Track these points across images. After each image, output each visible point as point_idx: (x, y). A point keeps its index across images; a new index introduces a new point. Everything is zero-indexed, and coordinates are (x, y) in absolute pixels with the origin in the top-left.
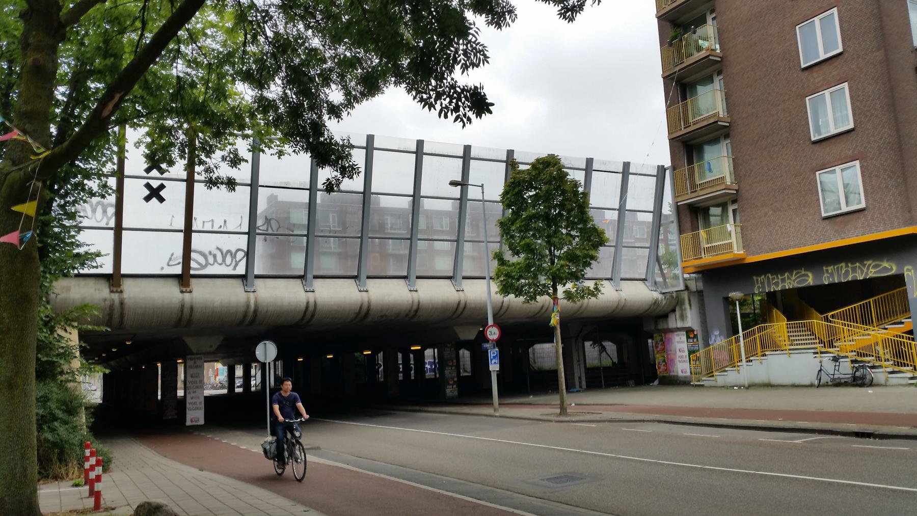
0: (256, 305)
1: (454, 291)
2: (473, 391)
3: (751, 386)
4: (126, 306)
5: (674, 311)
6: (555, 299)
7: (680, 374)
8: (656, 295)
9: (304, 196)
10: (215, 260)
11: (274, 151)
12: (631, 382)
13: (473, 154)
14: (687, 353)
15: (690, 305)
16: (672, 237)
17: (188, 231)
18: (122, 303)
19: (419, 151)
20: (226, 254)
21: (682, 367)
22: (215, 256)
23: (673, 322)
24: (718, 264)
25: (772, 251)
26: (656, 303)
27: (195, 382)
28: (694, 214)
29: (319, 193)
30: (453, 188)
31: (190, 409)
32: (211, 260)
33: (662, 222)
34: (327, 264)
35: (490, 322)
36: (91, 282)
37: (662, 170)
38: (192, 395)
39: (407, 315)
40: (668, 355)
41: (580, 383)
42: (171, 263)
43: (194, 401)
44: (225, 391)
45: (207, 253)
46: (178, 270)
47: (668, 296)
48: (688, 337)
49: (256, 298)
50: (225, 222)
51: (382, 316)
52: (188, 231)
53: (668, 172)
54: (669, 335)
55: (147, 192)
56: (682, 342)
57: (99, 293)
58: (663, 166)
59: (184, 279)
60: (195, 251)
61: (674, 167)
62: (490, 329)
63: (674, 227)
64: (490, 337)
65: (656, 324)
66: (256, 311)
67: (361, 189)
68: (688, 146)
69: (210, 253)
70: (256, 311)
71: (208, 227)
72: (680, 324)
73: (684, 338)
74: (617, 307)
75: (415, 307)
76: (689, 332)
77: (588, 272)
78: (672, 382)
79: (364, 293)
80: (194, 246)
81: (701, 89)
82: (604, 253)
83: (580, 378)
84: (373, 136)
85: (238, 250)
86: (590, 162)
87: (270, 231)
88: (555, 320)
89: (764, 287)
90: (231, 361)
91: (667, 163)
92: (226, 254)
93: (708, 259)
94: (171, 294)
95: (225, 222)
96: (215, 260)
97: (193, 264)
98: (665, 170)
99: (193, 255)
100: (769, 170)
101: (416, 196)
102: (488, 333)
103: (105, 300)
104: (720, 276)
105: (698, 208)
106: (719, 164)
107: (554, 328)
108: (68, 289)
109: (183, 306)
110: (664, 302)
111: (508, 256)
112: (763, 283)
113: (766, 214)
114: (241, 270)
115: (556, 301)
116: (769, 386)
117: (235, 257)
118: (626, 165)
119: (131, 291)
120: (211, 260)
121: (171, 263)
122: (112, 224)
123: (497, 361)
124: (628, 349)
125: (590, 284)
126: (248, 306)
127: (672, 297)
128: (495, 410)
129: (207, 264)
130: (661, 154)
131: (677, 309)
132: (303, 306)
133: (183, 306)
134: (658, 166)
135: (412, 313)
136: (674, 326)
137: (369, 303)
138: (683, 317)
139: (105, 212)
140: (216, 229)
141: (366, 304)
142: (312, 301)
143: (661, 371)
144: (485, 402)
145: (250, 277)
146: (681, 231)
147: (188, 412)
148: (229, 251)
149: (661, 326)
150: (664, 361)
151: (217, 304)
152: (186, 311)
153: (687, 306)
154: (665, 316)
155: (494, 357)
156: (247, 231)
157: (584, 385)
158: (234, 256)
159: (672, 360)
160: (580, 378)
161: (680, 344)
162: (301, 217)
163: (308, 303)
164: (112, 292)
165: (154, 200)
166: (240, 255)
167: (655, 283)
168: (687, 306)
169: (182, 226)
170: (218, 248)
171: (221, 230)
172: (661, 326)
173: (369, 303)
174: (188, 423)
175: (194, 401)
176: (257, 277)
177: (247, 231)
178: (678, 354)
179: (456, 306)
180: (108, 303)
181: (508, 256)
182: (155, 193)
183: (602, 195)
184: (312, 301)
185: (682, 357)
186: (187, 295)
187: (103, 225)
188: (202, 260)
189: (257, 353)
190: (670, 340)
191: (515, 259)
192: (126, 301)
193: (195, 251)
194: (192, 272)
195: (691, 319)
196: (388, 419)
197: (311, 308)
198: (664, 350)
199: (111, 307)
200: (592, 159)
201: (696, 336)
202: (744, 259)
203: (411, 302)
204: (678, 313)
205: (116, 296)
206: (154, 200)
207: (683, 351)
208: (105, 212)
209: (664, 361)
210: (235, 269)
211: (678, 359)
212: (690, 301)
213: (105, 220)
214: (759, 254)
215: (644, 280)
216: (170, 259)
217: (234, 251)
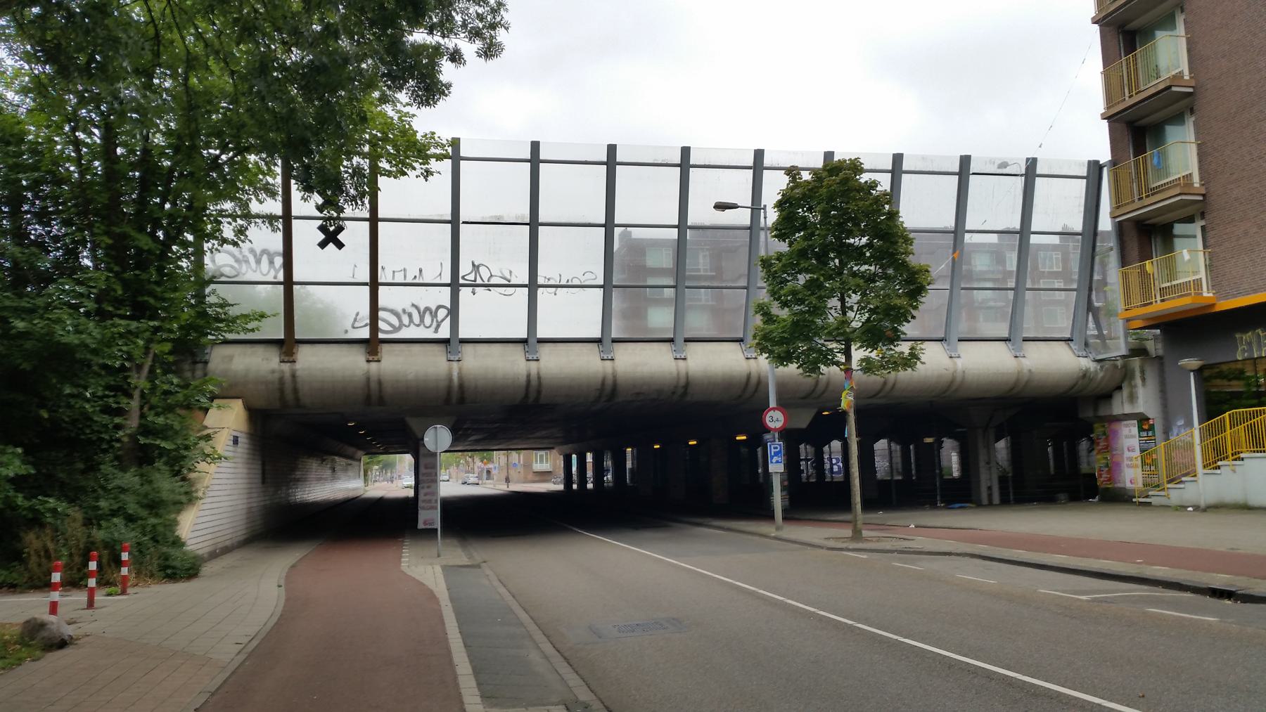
0: (460, 378)
1: (741, 356)
2: (742, 501)
3: (1217, 508)
4: (299, 380)
5: (1120, 388)
6: (848, 371)
7: (1128, 485)
8: (1086, 363)
9: (674, 233)
10: (411, 321)
11: (418, 172)
12: (1062, 496)
13: (767, 162)
14: (1137, 453)
15: (1143, 380)
16: (1112, 272)
17: (374, 284)
18: (294, 376)
19: (685, 163)
20: (425, 312)
21: (1131, 476)
22: (410, 315)
23: (1120, 406)
24: (1191, 310)
25: (1255, 291)
26: (1085, 375)
27: (430, 474)
28: (1147, 234)
29: (762, 234)
30: (719, 213)
31: (423, 508)
32: (406, 320)
33: (1097, 249)
34: (698, 323)
35: (773, 404)
36: (260, 349)
37: (1095, 169)
38: (426, 490)
39: (674, 393)
40: (1113, 456)
41: (990, 496)
42: (357, 325)
43: (428, 497)
44: (561, 487)
45: (400, 311)
46: (365, 333)
47: (1107, 365)
48: (1141, 429)
49: (460, 369)
50: (421, 271)
51: (638, 394)
52: (374, 284)
53: (1105, 170)
54: (1115, 426)
55: (322, 237)
56: (1133, 437)
57: (263, 363)
58: (1097, 162)
59: (372, 345)
60: (385, 309)
61: (1114, 163)
62: (771, 413)
63: (1113, 259)
64: (771, 425)
65: (1096, 409)
66: (461, 386)
67: (747, 222)
68: (1137, 127)
69: (404, 311)
70: (461, 386)
71: (399, 278)
72: (1128, 409)
73: (1135, 430)
74: (952, 382)
75: (682, 382)
76: (1142, 420)
77: (908, 329)
78: (1117, 497)
79: (608, 363)
80: (382, 302)
81: (1160, 34)
82: (933, 300)
83: (990, 488)
84: (689, 148)
85: (439, 307)
86: (898, 159)
87: (479, 281)
88: (847, 401)
89: (1251, 350)
90: (567, 448)
91: (1105, 155)
92: (425, 312)
93: (1158, 306)
94: (352, 364)
95: (421, 271)
96: (411, 321)
97: (381, 325)
98: (1101, 167)
99: (381, 314)
100: (1252, 160)
101: (682, 225)
102: (768, 419)
103: (273, 372)
104: (1189, 329)
105: (1154, 225)
106: (1182, 154)
107: (845, 413)
108: (231, 358)
109: (368, 379)
110: (1101, 375)
111: (776, 310)
112: (1250, 344)
113: (1246, 233)
114: (444, 333)
115: (851, 371)
116: (1245, 508)
117: (436, 316)
118: (965, 161)
119: (310, 361)
120: (406, 320)
121: (357, 325)
122: (281, 277)
123: (781, 458)
124: (1041, 446)
125: (904, 348)
126: (451, 380)
127: (1116, 366)
128: (778, 529)
129: (401, 325)
130: (1097, 143)
131: (1125, 385)
132: (523, 379)
133: (368, 379)
134: (1089, 162)
135: (680, 391)
136: (1120, 412)
137: (614, 376)
138: (1132, 398)
139: (271, 262)
140: (409, 280)
141: (610, 377)
142: (534, 372)
143: (1102, 481)
144: (822, 518)
145: (607, 341)
146: (1124, 261)
147: (420, 512)
148: (427, 309)
149: (1102, 412)
150: (1107, 465)
151: (411, 377)
152: (374, 385)
153: (1138, 381)
154: (1106, 396)
155: (776, 454)
156: (602, 283)
157: (996, 500)
158: (434, 315)
159: (1118, 465)
160: (990, 488)
161: (1129, 438)
162: (665, 260)
163: (529, 376)
164: (368, 361)
165: (331, 246)
166: (442, 313)
167: (1086, 344)
168: (1138, 381)
169: (366, 277)
170: (413, 305)
171: (417, 281)
172: (1102, 412)
173: (614, 376)
174: (421, 526)
175: (428, 497)
176: (615, 341)
177: (602, 283)
178: (1127, 454)
179: (744, 380)
180: (277, 375)
181: (776, 310)
182: (331, 237)
183: (922, 208)
184: (534, 372)
185: (1130, 459)
186: (374, 365)
187: (270, 278)
188: (395, 321)
189: (426, 439)
190: (1115, 433)
191: (784, 313)
192: (298, 373)
193: (385, 309)
194: (381, 336)
195: (1145, 399)
196: (648, 534)
197: (534, 382)
198: (1108, 448)
199: (281, 381)
200: (615, 146)
201: (1152, 428)
202: (1213, 305)
203: (675, 374)
204: (1125, 392)
205: (286, 367)
206: (331, 246)
207: (1133, 450)
208: (271, 262)
209: (1107, 465)
210: (436, 331)
211: (1126, 462)
212: (1143, 372)
213: (272, 273)
214: (1235, 296)
215: (1070, 340)
216: (355, 320)
217: (434, 309)
